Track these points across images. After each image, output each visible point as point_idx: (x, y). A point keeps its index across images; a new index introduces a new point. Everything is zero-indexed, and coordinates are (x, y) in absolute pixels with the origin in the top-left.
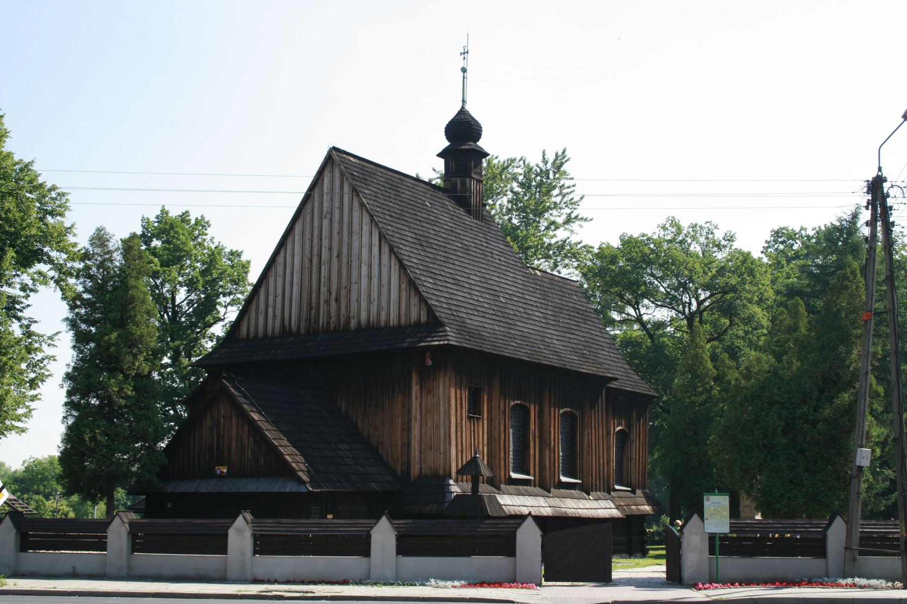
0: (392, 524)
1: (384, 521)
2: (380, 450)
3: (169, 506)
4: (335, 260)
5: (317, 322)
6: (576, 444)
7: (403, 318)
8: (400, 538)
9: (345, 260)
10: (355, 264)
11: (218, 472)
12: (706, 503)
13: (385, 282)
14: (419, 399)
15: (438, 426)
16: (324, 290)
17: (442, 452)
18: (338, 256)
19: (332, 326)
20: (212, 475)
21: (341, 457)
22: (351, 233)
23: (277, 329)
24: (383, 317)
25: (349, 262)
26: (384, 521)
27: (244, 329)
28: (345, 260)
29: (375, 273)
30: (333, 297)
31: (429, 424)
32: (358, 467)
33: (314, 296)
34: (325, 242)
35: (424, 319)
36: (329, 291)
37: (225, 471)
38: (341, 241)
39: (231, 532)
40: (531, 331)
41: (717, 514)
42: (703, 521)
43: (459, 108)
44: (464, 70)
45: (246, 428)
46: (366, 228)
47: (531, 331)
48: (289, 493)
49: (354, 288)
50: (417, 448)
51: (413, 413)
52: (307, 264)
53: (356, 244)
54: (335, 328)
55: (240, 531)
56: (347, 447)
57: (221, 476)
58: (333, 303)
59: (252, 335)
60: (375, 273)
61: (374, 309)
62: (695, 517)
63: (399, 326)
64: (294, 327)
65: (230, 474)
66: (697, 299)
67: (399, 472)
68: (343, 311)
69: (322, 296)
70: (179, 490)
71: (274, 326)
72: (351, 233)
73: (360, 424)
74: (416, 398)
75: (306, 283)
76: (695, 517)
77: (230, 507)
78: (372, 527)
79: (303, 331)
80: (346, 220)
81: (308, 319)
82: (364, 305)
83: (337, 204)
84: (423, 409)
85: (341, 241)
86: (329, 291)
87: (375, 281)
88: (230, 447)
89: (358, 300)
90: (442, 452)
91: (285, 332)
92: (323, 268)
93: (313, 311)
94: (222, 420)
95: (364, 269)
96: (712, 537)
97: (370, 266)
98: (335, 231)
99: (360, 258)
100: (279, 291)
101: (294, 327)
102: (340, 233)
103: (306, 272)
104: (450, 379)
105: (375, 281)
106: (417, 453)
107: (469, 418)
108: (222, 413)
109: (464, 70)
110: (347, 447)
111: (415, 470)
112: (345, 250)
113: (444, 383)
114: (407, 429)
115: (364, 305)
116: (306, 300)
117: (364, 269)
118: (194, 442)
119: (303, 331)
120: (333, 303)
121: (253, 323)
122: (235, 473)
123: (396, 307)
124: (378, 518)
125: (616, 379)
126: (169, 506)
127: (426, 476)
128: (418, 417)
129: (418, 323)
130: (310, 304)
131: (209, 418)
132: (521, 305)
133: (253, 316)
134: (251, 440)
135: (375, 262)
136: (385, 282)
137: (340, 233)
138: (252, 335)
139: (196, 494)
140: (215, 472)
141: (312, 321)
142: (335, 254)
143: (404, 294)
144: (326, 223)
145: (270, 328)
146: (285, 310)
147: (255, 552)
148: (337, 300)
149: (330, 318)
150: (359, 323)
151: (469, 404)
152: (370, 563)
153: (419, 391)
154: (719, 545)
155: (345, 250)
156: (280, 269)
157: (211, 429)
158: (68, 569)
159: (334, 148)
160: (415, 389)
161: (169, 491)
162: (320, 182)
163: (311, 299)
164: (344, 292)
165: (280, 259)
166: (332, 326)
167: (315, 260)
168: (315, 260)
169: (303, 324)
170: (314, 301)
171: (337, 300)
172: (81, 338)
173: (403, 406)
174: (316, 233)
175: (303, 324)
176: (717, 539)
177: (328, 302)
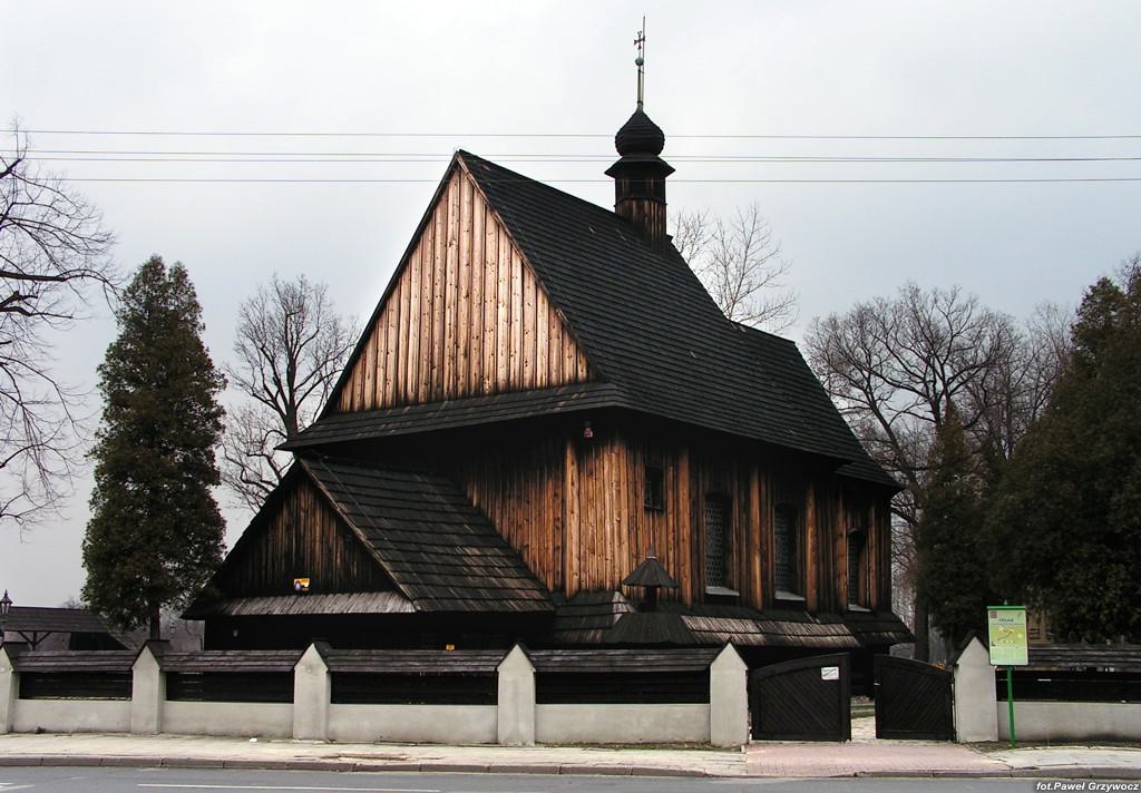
0: (528, 656)
1: (517, 653)
2: (526, 556)
3: (235, 634)
4: (463, 302)
5: (440, 385)
6: (795, 548)
7: (554, 375)
8: (541, 679)
9: (476, 300)
10: (490, 306)
11: (298, 586)
12: (991, 621)
13: (529, 326)
14: (576, 485)
15: (603, 522)
16: (449, 342)
17: (609, 557)
18: (467, 296)
19: (460, 389)
20: (289, 590)
21: (467, 566)
22: (484, 263)
23: (389, 397)
24: (528, 375)
25: (483, 303)
26: (517, 653)
27: (347, 399)
28: (476, 300)
29: (517, 314)
30: (461, 350)
31: (591, 519)
32: (493, 579)
33: (436, 350)
34: (451, 278)
35: (582, 374)
36: (456, 343)
37: (307, 584)
38: (471, 275)
39: (299, 670)
40: (732, 396)
41: (1010, 638)
42: (988, 649)
43: (633, 109)
44: (640, 63)
45: (334, 527)
46: (504, 256)
47: (732, 396)
48: (389, 614)
49: (489, 337)
50: (575, 552)
51: (568, 504)
52: (427, 308)
53: (491, 277)
54: (464, 391)
55: (310, 667)
56: (477, 552)
57: (301, 593)
58: (461, 359)
59: (356, 406)
60: (517, 314)
61: (515, 365)
62: (975, 643)
63: (549, 385)
64: (411, 394)
65: (314, 590)
66: (943, 379)
67: (550, 587)
68: (474, 369)
69: (447, 350)
70: (244, 613)
71: (385, 393)
72: (484, 263)
73: (498, 521)
74: (573, 484)
75: (426, 334)
76: (975, 643)
77: (297, 633)
78: (501, 661)
79: (422, 398)
80: (477, 246)
81: (429, 382)
82: (502, 360)
83: (465, 225)
84: (582, 496)
85: (471, 275)
86: (456, 343)
87: (517, 326)
88: (313, 552)
89: (495, 354)
90: (609, 557)
91: (400, 400)
92: (448, 312)
93: (435, 371)
94: (302, 514)
95: (503, 312)
96: (1001, 673)
97: (510, 307)
98: (464, 262)
99: (496, 297)
100: (392, 346)
101: (411, 394)
102: (470, 264)
103: (426, 318)
104: (618, 455)
105: (517, 326)
106: (575, 562)
107: (647, 510)
108: (303, 504)
109: (640, 63)
110: (477, 552)
111: (572, 583)
112: (476, 286)
113: (610, 461)
114: (561, 525)
115: (502, 360)
116: (425, 357)
117: (503, 312)
118: (267, 545)
119: (422, 398)
120: (461, 359)
121: (358, 390)
122: (321, 588)
123: (545, 361)
124: (509, 648)
125: (849, 462)
126: (235, 634)
127: (587, 591)
128: (576, 511)
129: (575, 381)
130: (432, 362)
131: (285, 513)
132: (719, 363)
133: (358, 381)
134: (341, 543)
135: (517, 301)
136: (529, 326)
137: (470, 264)
138: (356, 406)
139: (269, 617)
140: (294, 587)
141: (435, 385)
142: (464, 293)
143: (555, 341)
144: (452, 251)
145: (380, 396)
146: (397, 369)
147: (333, 701)
148: (467, 355)
149: (458, 379)
150: (496, 384)
151: (647, 492)
152: (292, 711)
153: (575, 474)
154: (1014, 685)
155: (476, 286)
156: (393, 316)
157: (289, 528)
158: (194, 726)
159: (462, 152)
160: (571, 470)
161: (233, 613)
162: (444, 198)
163: (432, 354)
164: (475, 344)
165: (393, 304)
166: (460, 389)
167: (438, 301)
168: (438, 301)
169: (422, 388)
170: (436, 356)
171: (467, 355)
172: (117, 402)
173: (556, 495)
174: (438, 266)
175: (422, 388)
176: (1009, 674)
177: (454, 358)
